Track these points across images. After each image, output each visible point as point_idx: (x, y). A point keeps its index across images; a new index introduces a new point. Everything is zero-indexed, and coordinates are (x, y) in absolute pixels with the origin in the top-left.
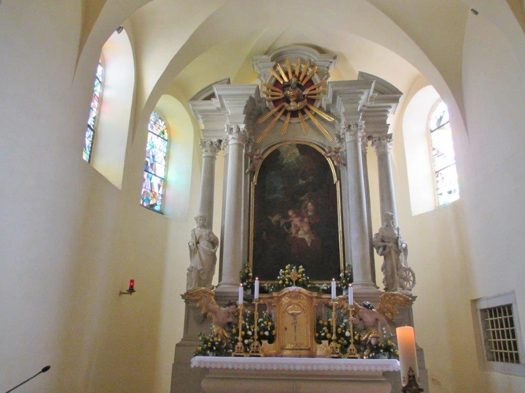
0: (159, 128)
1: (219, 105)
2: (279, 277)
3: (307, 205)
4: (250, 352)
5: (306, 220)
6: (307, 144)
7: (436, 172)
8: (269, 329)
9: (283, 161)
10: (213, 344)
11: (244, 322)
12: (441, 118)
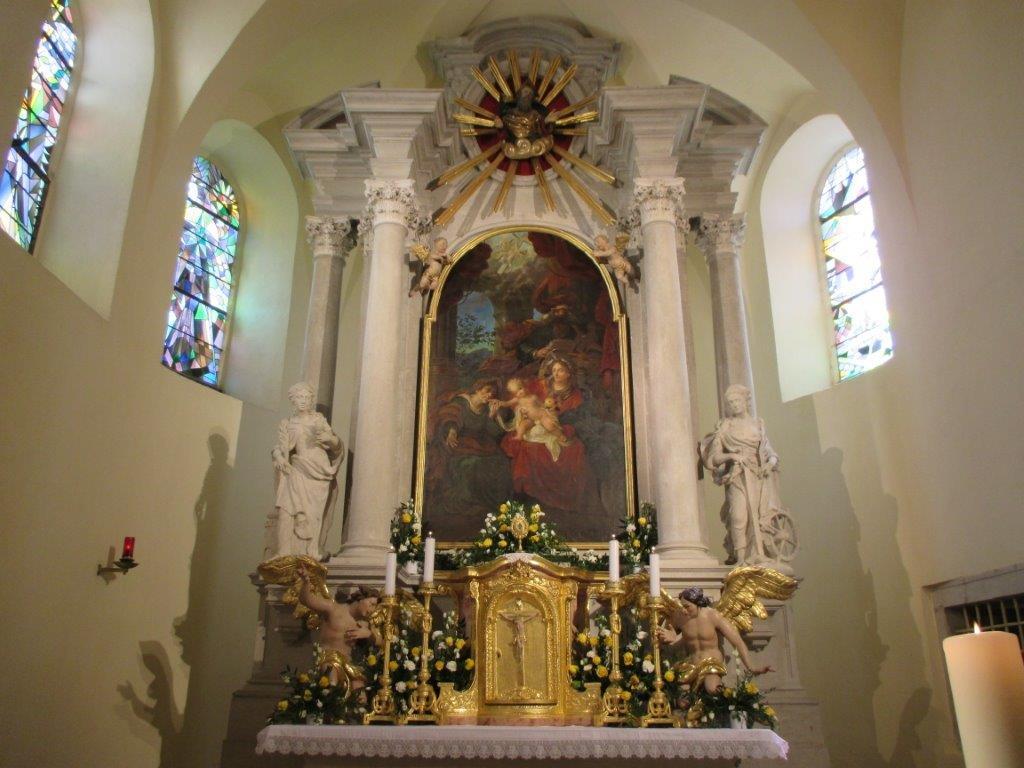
0: (218, 200)
1: (353, 141)
2: (483, 531)
4: (411, 711)
5: (548, 402)
6: (554, 233)
7: (834, 308)
8: (458, 656)
9: (497, 269)
10: (317, 692)
11: (395, 639)
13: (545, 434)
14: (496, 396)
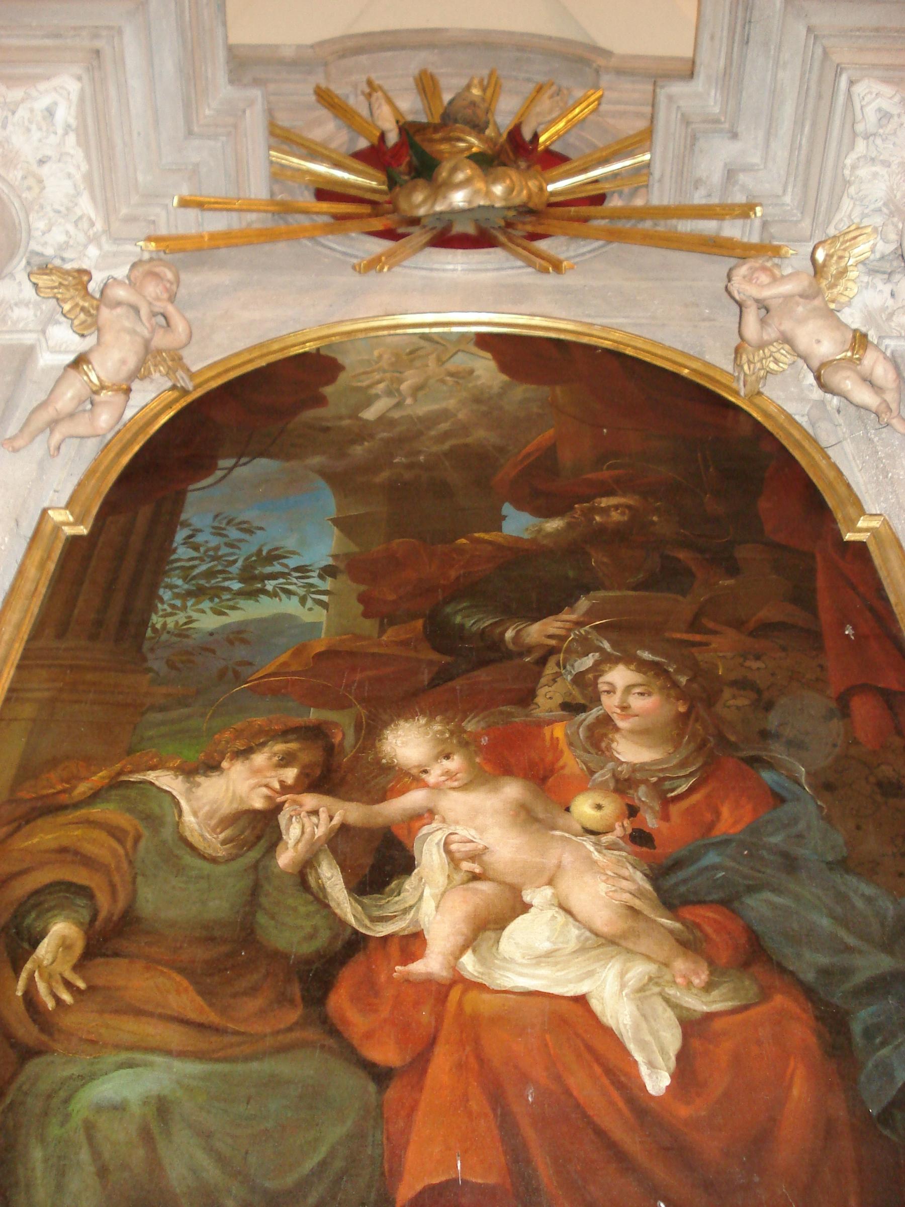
13: (582, 950)
14: (323, 779)
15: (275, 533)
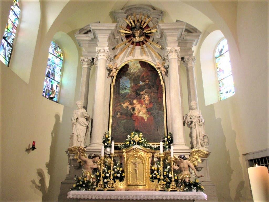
0: (57, 53)
1: (93, 37)
2: (127, 140)
3: (144, 97)
4: (108, 187)
5: (144, 106)
7: (219, 81)
8: (120, 172)
10: (83, 182)
11: (104, 168)
12: (222, 50)
14: (130, 104)
15: (127, 85)
